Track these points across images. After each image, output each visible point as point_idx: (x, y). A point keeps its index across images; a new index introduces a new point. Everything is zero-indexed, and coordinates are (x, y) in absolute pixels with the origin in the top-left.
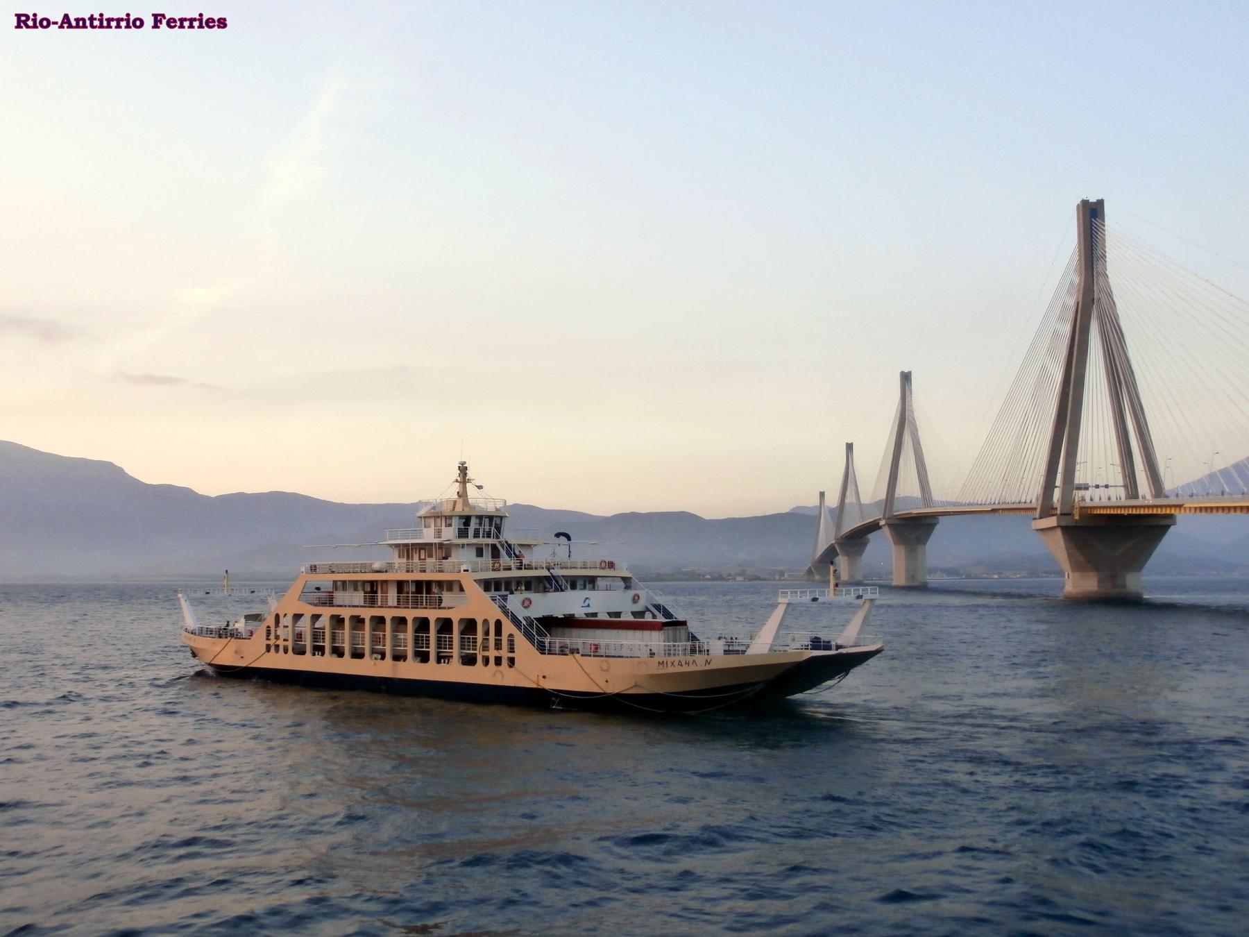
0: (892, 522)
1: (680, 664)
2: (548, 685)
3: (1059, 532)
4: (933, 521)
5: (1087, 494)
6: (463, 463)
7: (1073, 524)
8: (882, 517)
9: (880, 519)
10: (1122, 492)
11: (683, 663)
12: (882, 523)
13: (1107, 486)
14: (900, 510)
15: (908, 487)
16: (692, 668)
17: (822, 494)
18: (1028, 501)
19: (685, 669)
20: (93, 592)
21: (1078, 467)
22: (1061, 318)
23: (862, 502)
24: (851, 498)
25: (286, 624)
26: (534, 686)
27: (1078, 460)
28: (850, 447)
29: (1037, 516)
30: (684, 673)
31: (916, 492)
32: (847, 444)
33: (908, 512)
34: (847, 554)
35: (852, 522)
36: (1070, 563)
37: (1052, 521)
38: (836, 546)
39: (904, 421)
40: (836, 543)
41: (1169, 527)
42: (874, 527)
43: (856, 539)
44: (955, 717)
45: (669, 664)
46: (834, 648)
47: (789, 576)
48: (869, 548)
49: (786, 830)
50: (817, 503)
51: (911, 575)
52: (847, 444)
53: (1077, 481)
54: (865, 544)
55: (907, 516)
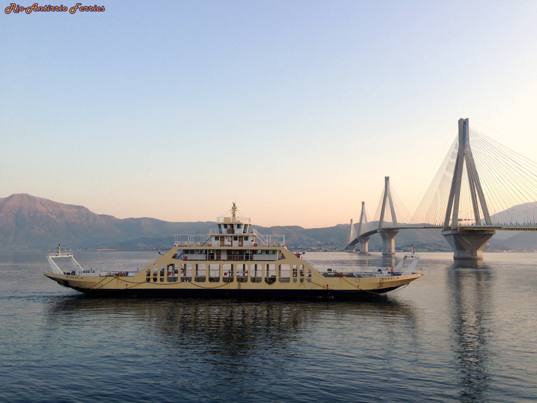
1: (389, 279)
2: (330, 288)
5: (460, 222)
9: (377, 230)
10: (474, 222)
11: (390, 278)
13: (465, 220)
14: (384, 226)
15: (388, 219)
16: (393, 280)
17: (352, 220)
18: (438, 225)
19: (390, 280)
20: (502, 184)
21: (459, 213)
22: (452, 157)
23: (398, 222)
24: (364, 222)
26: (356, 289)
28: (363, 203)
30: (388, 282)
32: (362, 202)
35: (363, 232)
36: (456, 247)
39: (386, 193)
41: (492, 235)
42: (375, 232)
43: (366, 237)
45: (385, 279)
46: (155, 277)
52: (362, 202)
53: (459, 218)
55: (131, 253)
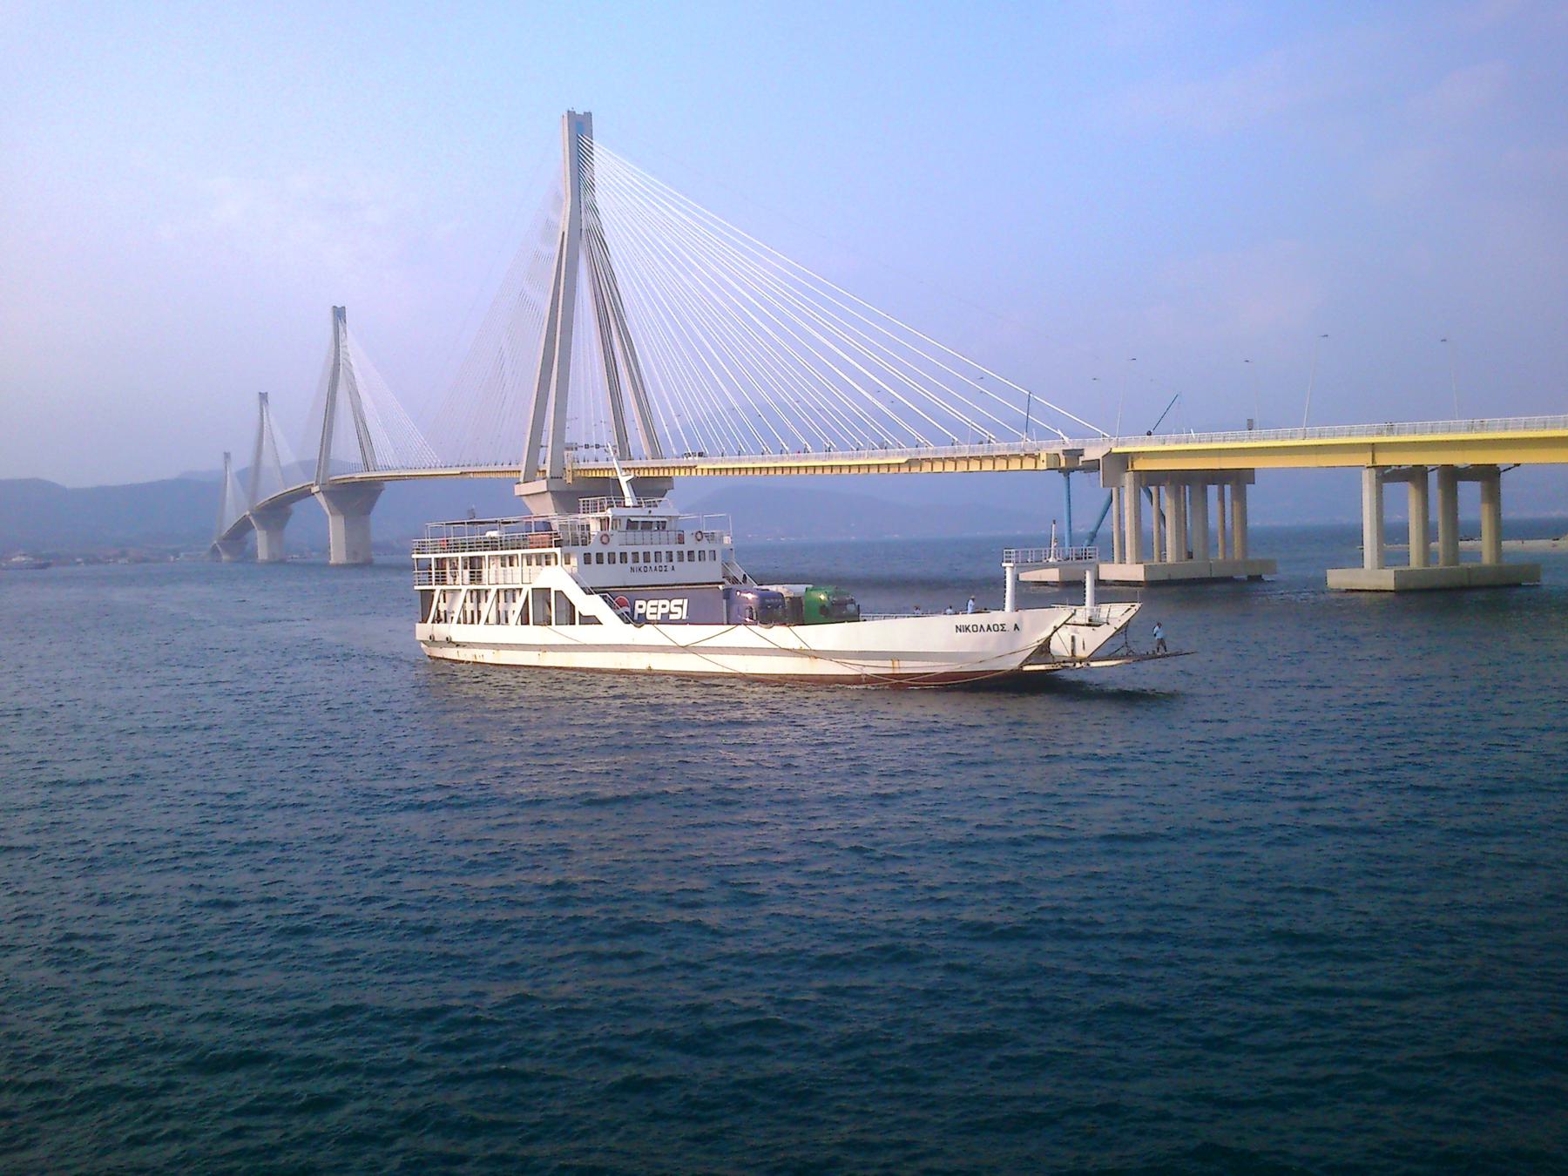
0: (327, 488)
3: (549, 496)
4: (666, 486)
6: (1252, 420)
7: (565, 489)
8: (314, 482)
12: (315, 489)
15: (346, 452)
25: (1025, 627)
27: (568, 416)
29: (522, 480)
31: (355, 457)
33: (348, 476)
34: (265, 526)
37: (541, 486)
38: (251, 518)
40: (252, 514)
43: (276, 511)
44: (1314, 810)
47: (187, 556)
48: (292, 522)
49: (224, 1031)
50: (1376, 455)
51: (352, 551)
53: (567, 440)
54: (287, 516)
